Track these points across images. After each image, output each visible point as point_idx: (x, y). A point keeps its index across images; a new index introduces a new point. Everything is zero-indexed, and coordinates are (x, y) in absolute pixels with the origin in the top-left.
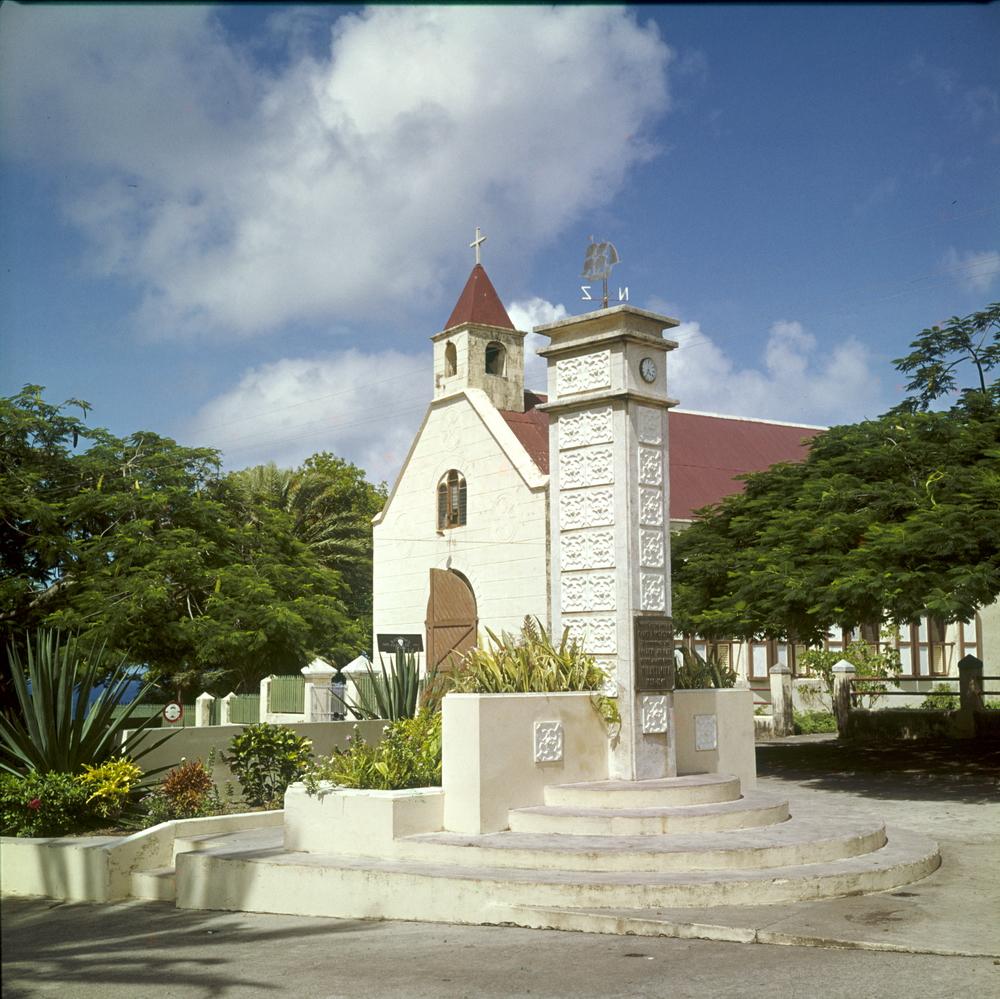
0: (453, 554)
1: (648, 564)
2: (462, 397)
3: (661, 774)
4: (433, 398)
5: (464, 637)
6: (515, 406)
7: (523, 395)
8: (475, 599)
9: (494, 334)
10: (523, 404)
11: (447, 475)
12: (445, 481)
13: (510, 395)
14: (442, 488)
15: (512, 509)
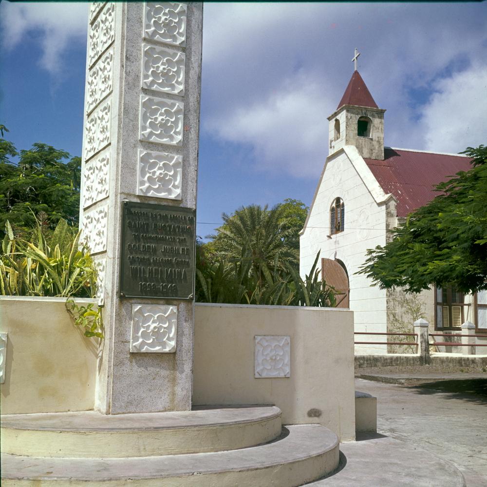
0: (337, 249)
1: (153, 139)
2: (342, 151)
3: (160, 407)
4: (328, 155)
5: (341, 301)
6: (378, 156)
7: (383, 149)
8: (348, 277)
9: (363, 112)
10: (383, 154)
11: (335, 201)
12: (334, 205)
13: (374, 149)
14: (332, 210)
15: (368, 218)
